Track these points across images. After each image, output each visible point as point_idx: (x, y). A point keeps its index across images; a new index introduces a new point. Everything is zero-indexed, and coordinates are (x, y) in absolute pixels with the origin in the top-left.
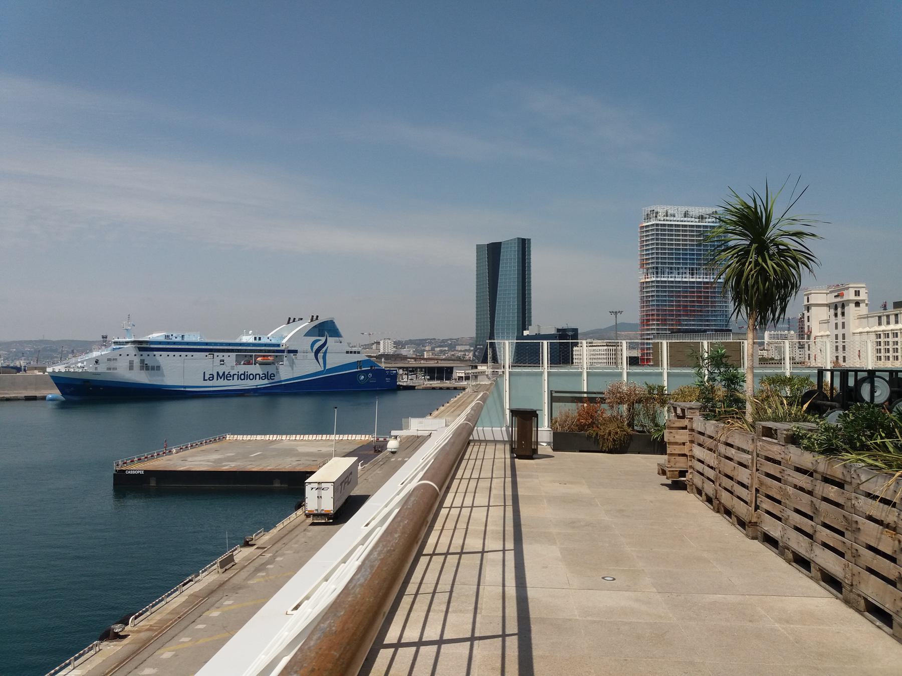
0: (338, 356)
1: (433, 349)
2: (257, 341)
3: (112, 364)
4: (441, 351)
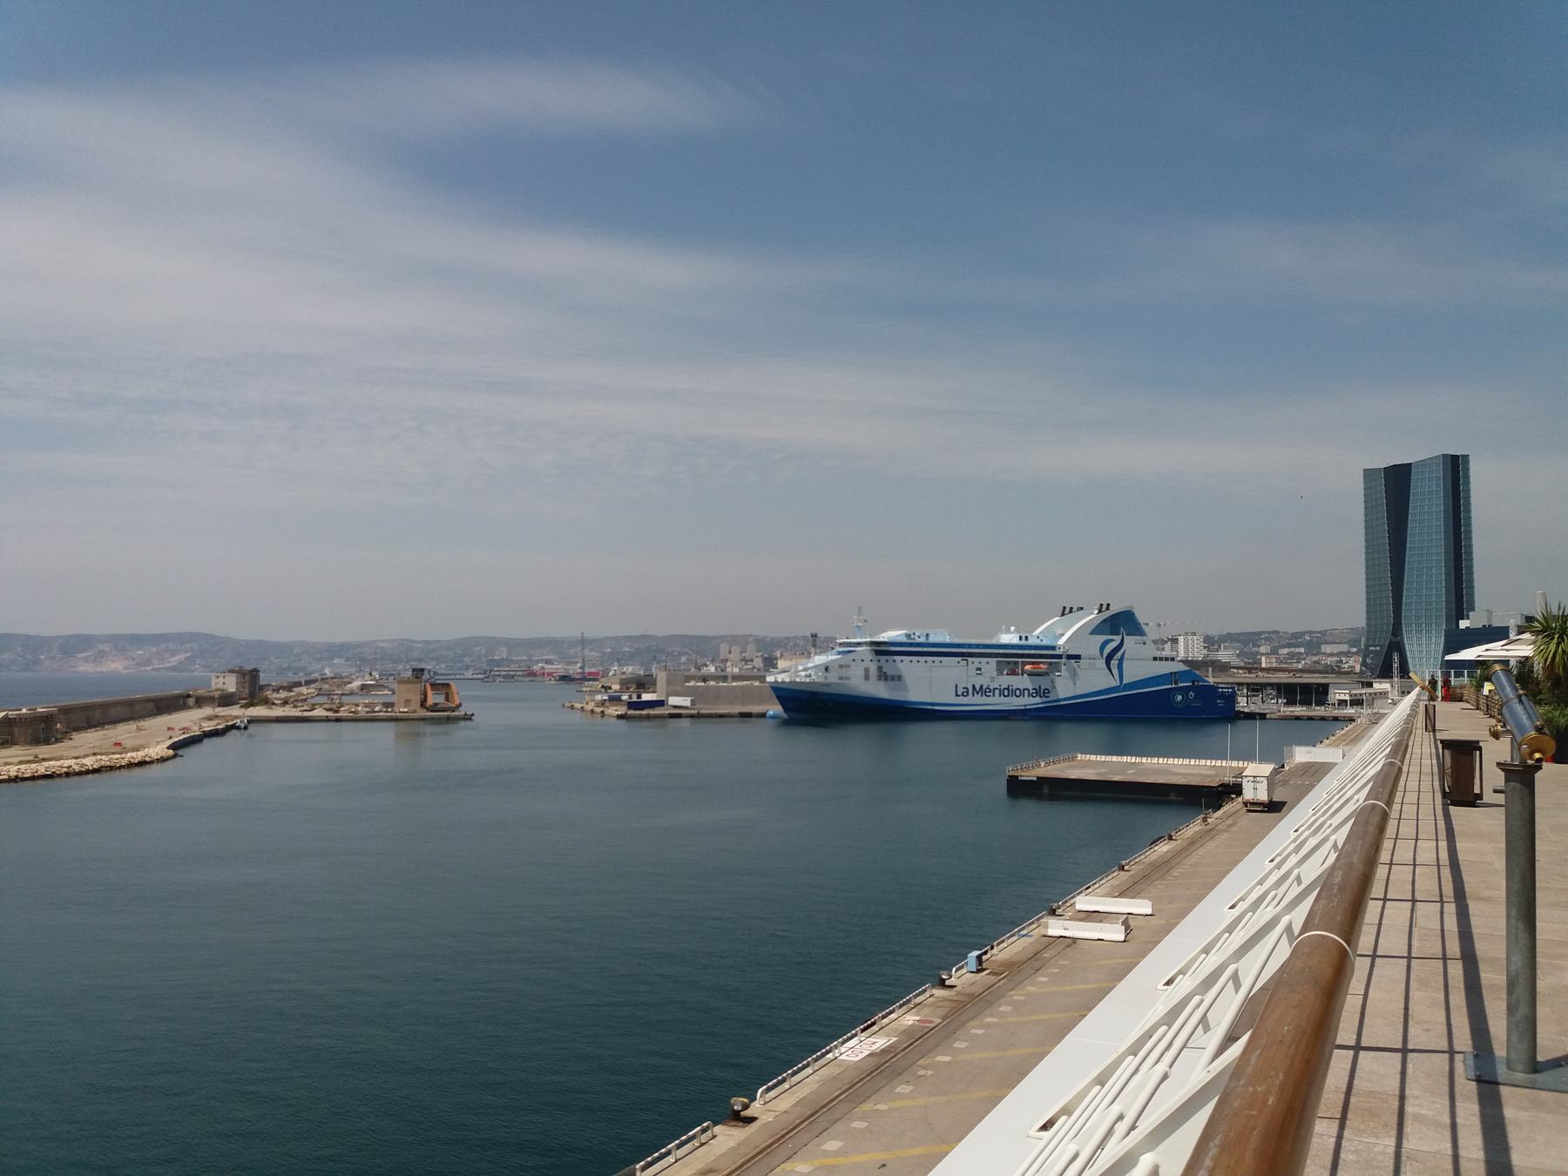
1: (1274, 652)
2: (1023, 642)
3: (844, 672)
4: (1292, 655)
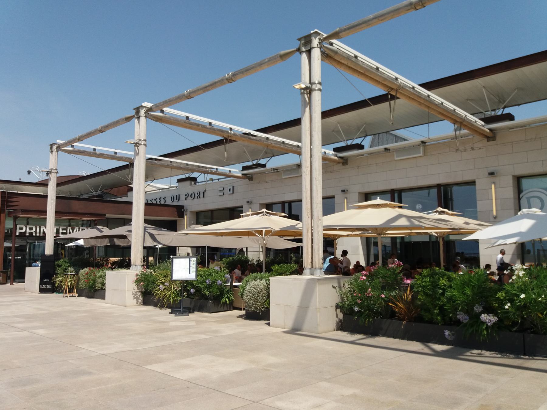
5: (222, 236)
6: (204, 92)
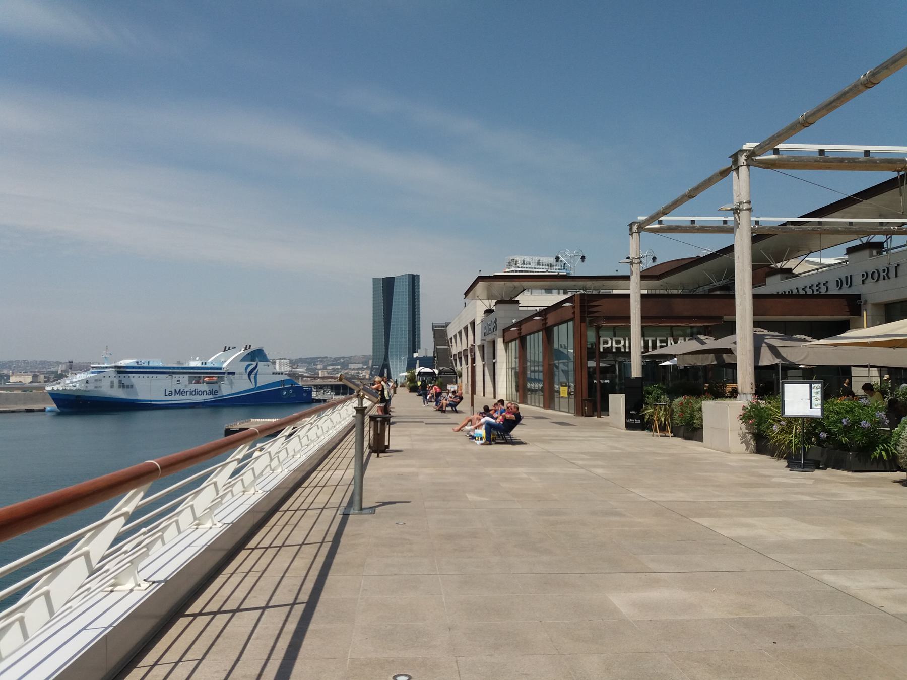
0: (266, 376)
1: (325, 368)
3: (98, 384)
4: (334, 370)
5: (894, 347)
6: (829, 111)
